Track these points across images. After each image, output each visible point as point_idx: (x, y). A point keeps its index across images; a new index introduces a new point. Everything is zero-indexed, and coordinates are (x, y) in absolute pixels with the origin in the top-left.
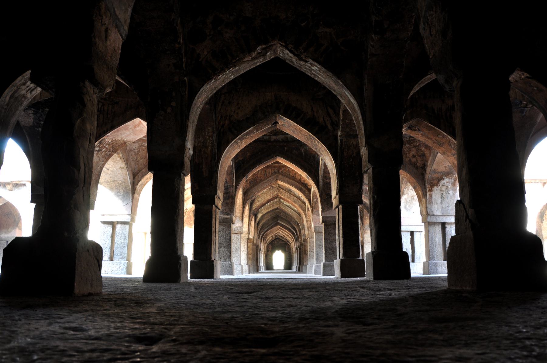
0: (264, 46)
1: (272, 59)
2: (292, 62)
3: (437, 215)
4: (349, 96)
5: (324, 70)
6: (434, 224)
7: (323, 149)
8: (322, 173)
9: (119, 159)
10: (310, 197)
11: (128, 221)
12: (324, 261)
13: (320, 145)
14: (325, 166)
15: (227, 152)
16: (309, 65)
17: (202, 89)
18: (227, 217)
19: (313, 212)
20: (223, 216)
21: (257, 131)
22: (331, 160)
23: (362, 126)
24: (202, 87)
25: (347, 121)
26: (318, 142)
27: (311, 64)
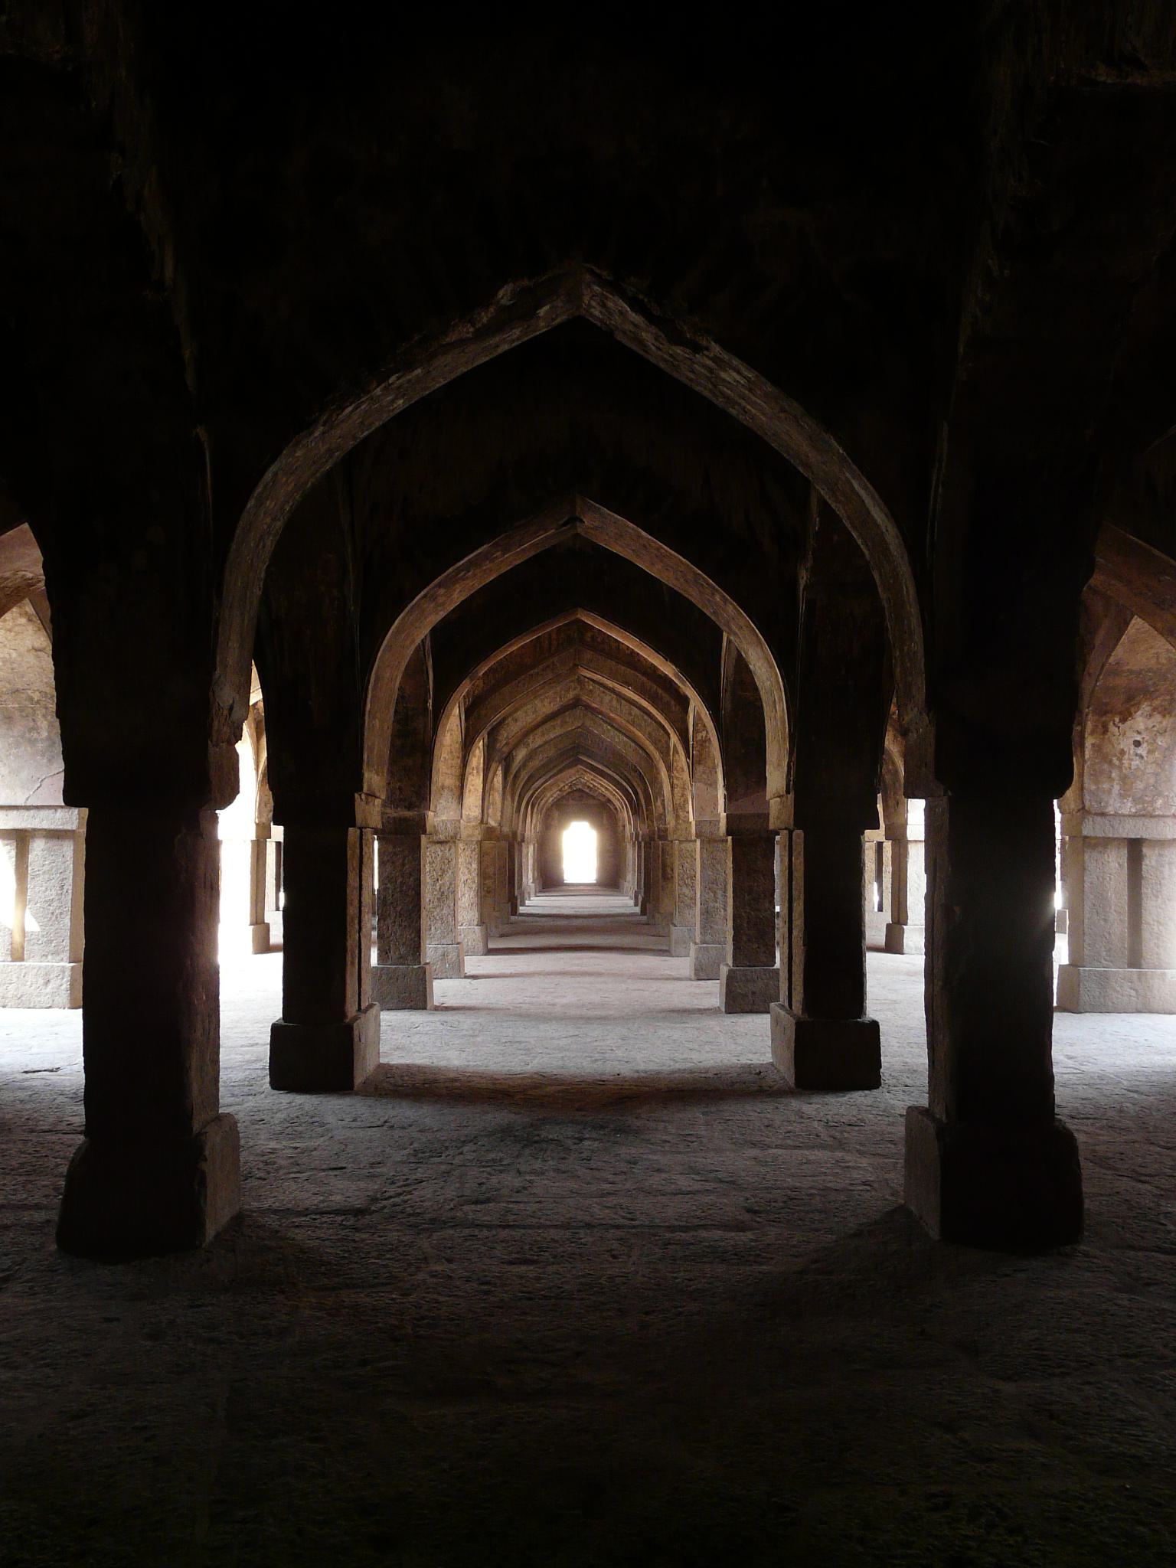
0: (526, 283)
1: (559, 326)
2: (641, 343)
3: (1116, 815)
4: (868, 501)
5: (769, 388)
6: (1104, 843)
8: (731, 670)
9: (23, 621)
11: (68, 827)
12: (730, 962)
13: (730, 608)
14: (741, 665)
16: (709, 363)
17: (273, 468)
21: (505, 551)
22: (771, 667)
23: (913, 610)
24: (272, 461)
26: (725, 601)
27: (716, 360)
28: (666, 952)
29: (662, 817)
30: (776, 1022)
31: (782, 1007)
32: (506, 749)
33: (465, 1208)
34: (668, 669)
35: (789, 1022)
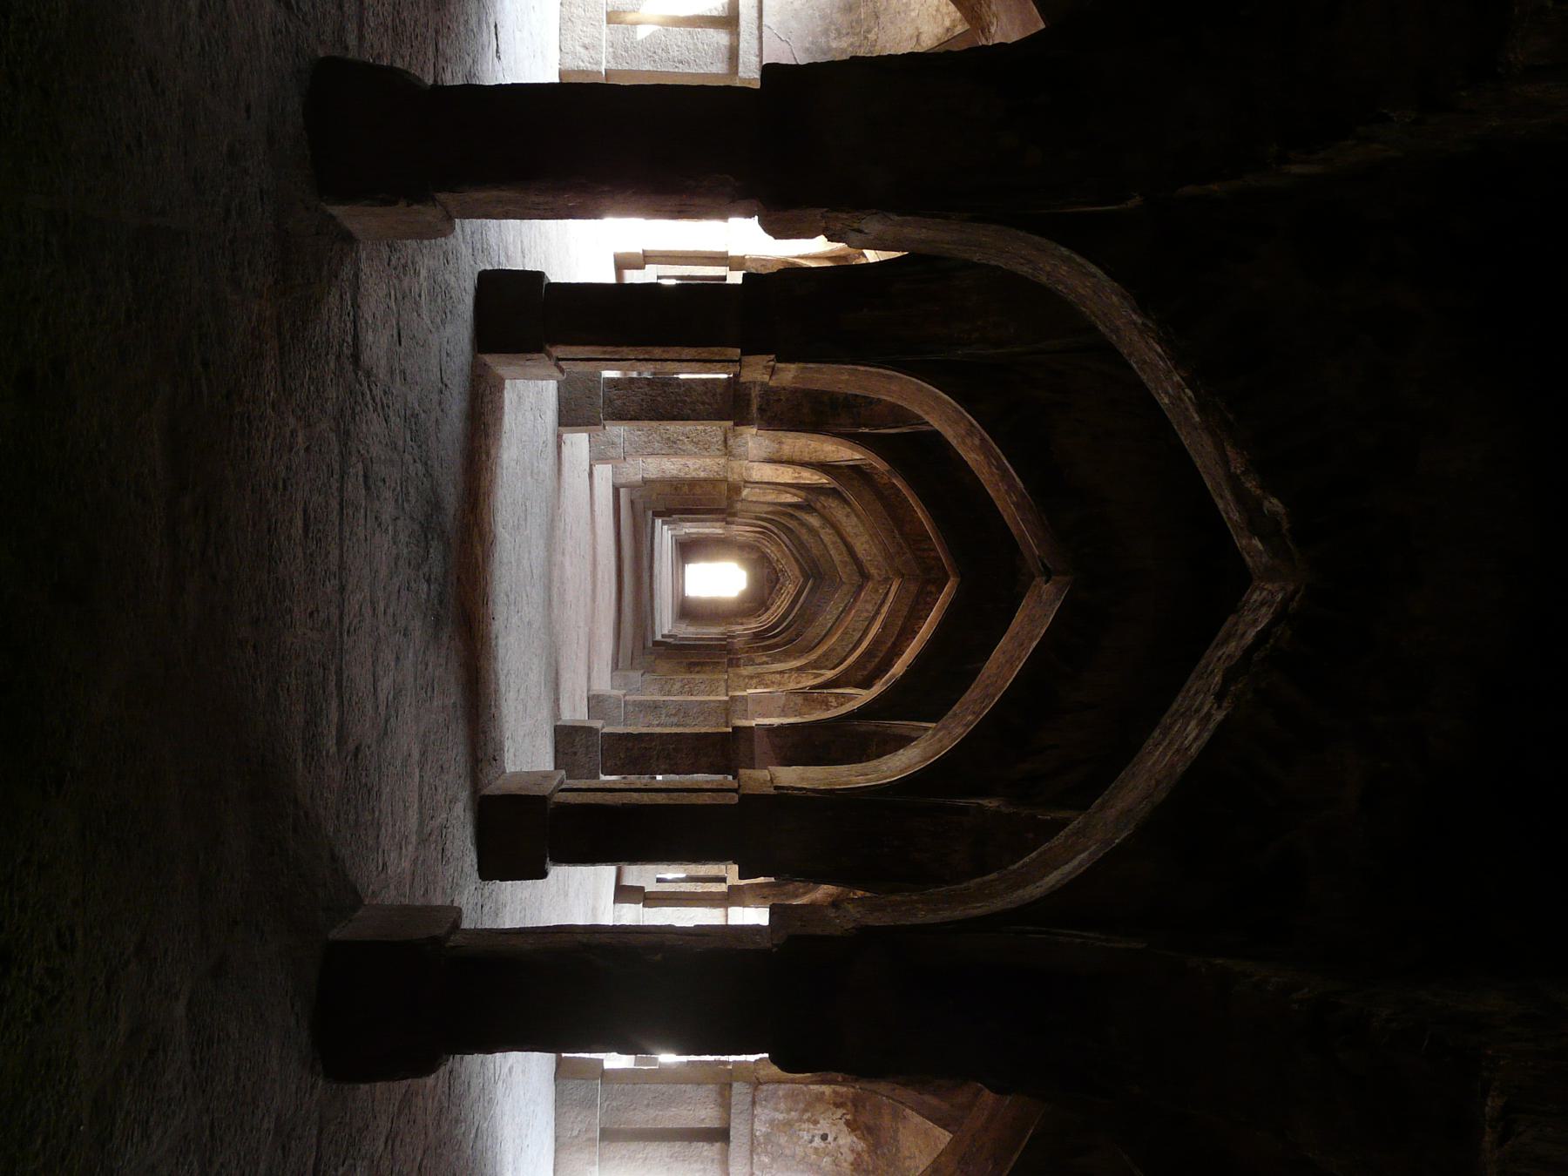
0: (1285, 526)
3: (753, 1116)
4: (1067, 868)
5: (1180, 769)
6: (725, 1104)
7: (945, 742)
9: (947, 23)
10: (846, 685)
13: (959, 730)
14: (903, 741)
15: (938, 398)
16: (1206, 709)
17: (1099, 273)
18: (754, 408)
19: (794, 693)
20: (755, 392)
21: (1017, 505)
22: (901, 771)
23: (958, 913)
24: (1107, 272)
25: (1031, 835)
27: (1209, 715)
28: (616, 666)
29: (751, 662)
30: (546, 776)
31: (561, 782)
32: (818, 506)
33: (360, 466)
34: (899, 668)
35: (546, 789)
